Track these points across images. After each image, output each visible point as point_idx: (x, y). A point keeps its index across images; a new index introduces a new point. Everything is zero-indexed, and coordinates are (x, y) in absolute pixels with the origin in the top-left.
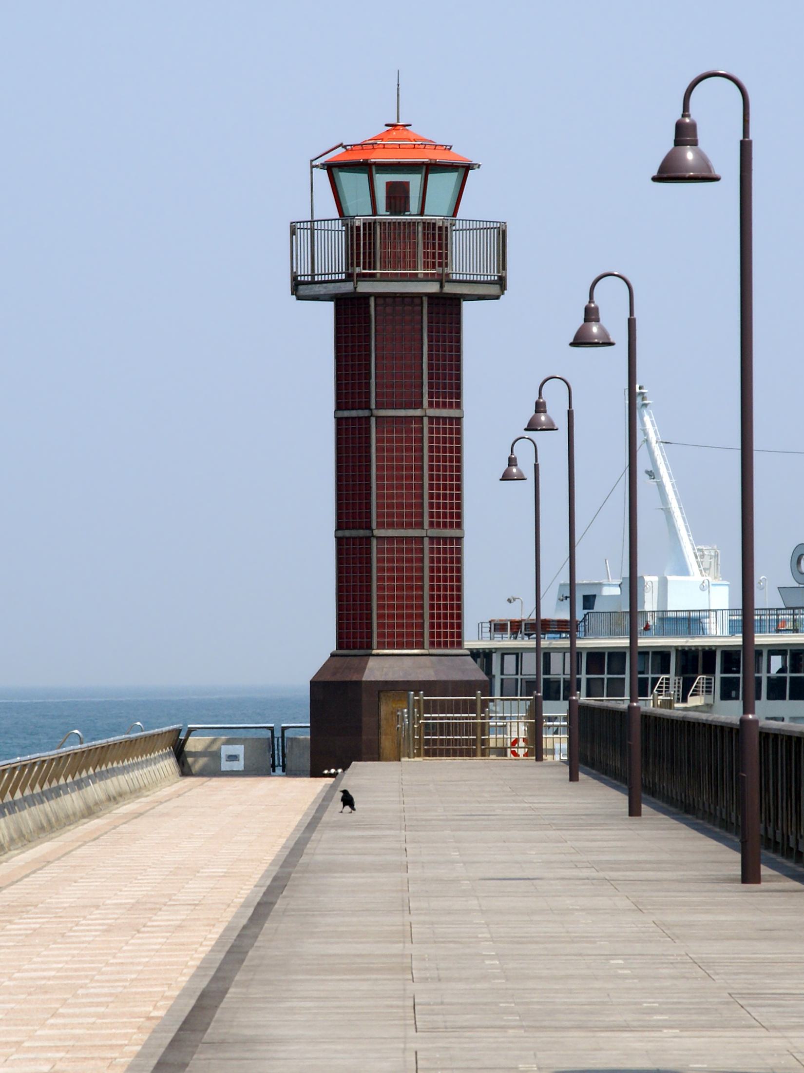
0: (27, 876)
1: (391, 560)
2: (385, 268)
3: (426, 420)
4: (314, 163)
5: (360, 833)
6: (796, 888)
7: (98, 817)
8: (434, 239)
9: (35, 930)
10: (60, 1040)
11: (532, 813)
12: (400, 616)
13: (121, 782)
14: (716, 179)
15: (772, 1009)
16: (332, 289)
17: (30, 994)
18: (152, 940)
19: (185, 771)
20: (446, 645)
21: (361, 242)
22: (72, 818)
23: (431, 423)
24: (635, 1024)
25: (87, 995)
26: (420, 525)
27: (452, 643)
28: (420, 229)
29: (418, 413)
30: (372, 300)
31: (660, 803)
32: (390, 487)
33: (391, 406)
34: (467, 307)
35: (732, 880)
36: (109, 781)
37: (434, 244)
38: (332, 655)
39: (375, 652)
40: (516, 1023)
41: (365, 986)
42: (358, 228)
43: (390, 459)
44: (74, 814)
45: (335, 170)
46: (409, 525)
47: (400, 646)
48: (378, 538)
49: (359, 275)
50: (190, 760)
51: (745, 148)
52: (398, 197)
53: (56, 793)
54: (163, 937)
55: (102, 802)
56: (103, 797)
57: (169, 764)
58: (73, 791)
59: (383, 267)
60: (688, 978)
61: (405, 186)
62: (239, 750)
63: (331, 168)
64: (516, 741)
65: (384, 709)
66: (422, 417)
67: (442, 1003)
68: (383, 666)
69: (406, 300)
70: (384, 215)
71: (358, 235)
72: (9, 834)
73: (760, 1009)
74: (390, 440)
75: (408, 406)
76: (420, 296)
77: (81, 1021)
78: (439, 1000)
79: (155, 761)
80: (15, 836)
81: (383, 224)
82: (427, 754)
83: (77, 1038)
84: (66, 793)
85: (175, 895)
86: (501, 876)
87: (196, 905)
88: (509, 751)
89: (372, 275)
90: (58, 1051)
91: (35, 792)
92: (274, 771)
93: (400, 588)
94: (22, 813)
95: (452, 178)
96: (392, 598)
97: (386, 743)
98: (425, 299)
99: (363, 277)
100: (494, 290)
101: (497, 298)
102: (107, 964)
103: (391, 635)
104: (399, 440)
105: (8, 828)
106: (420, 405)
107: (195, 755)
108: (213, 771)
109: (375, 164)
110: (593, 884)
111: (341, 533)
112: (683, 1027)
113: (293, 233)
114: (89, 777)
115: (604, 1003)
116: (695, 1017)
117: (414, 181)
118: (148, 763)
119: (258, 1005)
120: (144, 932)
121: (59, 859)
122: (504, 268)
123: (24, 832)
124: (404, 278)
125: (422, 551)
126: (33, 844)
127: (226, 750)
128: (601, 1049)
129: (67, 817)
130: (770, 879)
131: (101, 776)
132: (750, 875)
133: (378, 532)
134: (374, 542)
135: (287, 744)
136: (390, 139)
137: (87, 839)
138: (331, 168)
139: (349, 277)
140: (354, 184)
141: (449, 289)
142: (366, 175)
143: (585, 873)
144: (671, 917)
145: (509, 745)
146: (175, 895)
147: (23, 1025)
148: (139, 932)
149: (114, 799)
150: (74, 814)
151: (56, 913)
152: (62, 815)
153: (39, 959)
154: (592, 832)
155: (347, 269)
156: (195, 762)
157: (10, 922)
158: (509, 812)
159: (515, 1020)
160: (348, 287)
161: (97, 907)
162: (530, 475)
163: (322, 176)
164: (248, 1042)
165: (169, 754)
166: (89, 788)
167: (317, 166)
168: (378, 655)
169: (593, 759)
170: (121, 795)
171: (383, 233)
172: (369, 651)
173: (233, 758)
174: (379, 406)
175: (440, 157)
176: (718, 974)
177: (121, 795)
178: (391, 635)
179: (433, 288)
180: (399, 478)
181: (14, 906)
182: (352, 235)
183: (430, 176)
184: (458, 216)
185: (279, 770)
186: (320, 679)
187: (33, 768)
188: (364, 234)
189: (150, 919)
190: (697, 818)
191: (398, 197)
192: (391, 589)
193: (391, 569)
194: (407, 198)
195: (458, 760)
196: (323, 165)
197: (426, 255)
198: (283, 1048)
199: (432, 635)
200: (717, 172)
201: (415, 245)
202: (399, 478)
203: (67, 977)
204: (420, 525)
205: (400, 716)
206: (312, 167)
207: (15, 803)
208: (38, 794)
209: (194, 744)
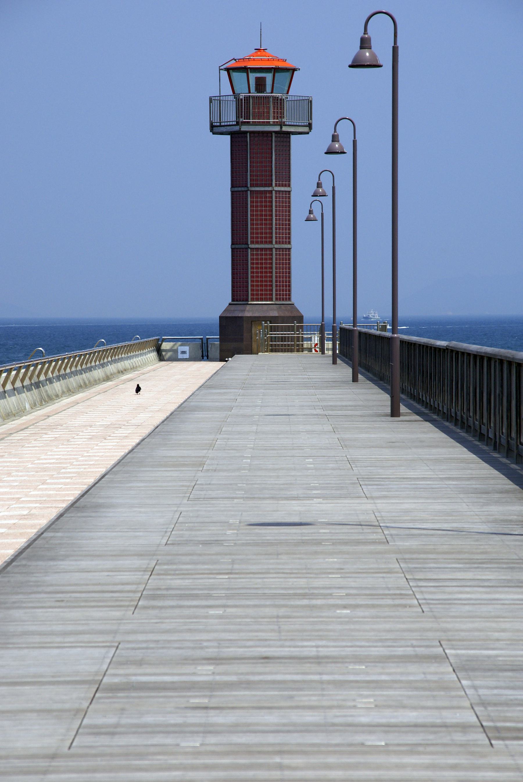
0: (64, 410)
1: (257, 259)
2: (254, 119)
3: (274, 192)
4: (221, 68)
5: (219, 391)
6: (416, 419)
7: (111, 381)
8: (278, 105)
9: (56, 438)
10: (40, 497)
11: (308, 380)
12: (261, 286)
13: (126, 364)
14: (380, 66)
15: (375, 487)
16: (229, 129)
17: (37, 472)
18: (108, 444)
19: (161, 358)
20: (283, 300)
21: (243, 106)
22: (98, 381)
23: (276, 194)
24: (302, 496)
25: (65, 473)
26: (271, 242)
27: (286, 299)
28: (271, 100)
29: (270, 189)
30: (248, 134)
31: (371, 375)
32: (257, 224)
33: (257, 185)
34: (293, 137)
35: (387, 415)
36: (119, 364)
37: (278, 107)
38: (230, 304)
39: (250, 303)
40: (241, 496)
41: (175, 474)
42: (242, 99)
43: (257, 211)
44: (99, 379)
45: (231, 71)
46: (266, 243)
47: (262, 300)
48: (251, 249)
49: (242, 122)
50: (164, 353)
51: (395, 50)
52: (260, 85)
53: (90, 369)
54: (115, 442)
55: (114, 374)
56: (115, 371)
57: (153, 355)
58: (99, 368)
59: (253, 118)
60: (340, 469)
61: (264, 79)
62: (186, 349)
63: (228, 70)
64: (317, 344)
65: (253, 330)
66: (272, 191)
67: (210, 484)
68: (254, 309)
69: (260, 134)
70: (254, 93)
71: (242, 103)
72: (62, 389)
73: (369, 487)
74: (257, 202)
75: (266, 185)
76: (271, 132)
77: (55, 486)
78: (209, 482)
79: (145, 354)
80: (65, 390)
81: (253, 97)
82: (272, 351)
83: (49, 496)
84: (95, 369)
85: (131, 420)
86: (276, 413)
87: (139, 425)
88: (313, 349)
89: (248, 122)
90: (36, 503)
91: (78, 369)
92: (203, 358)
93: (262, 272)
94: (70, 379)
95: (288, 75)
96: (257, 277)
97: (254, 346)
98: (274, 134)
99: (244, 123)
100: (306, 129)
101: (308, 133)
102: (82, 456)
103: (257, 295)
104: (261, 202)
105: (61, 386)
106: (271, 185)
107: (166, 351)
108: (174, 359)
109: (250, 68)
110: (318, 418)
111: (234, 246)
112: (324, 497)
113: (211, 101)
114: (108, 362)
115: (291, 484)
116: (333, 492)
117: (269, 77)
118: (141, 355)
119: (116, 485)
120: (108, 440)
121: (84, 401)
122: (311, 119)
123: (71, 388)
124: (263, 124)
125: (272, 255)
126: (74, 394)
127: (181, 349)
128: (278, 511)
129: (95, 381)
130: (405, 415)
131: (115, 361)
132: (395, 413)
133: (250, 246)
134: (249, 250)
135: (210, 346)
136: (257, 56)
137: (101, 392)
138: (228, 70)
139: (238, 123)
140: (239, 78)
141: (285, 129)
142: (246, 74)
143: (318, 411)
144: (347, 436)
145: (313, 346)
146: (131, 420)
147: (26, 489)
148: (105, 439)
149: (122, 372)
150: (99, 379)
151: (70, 429)
152: (92, 380)
153: (97, 447)
154: (331, 390)
155: (236, 119)
156: (166, 355)
157: (46, 434)
158: (297, 380)
159: (242, 494)
160: (236, 128)
161: (91, 426)
162: (319, 218)
163: (225, 74)
164: (97, 507)
165: (153, 351)
166: (108, 367)
167: (222, 69)
168: (251, 304)
169: (347, 353)
170: (125, 370)
171: (254, 103)
172: (247, 302)
173: (184, 352)
174: (252, 185)
175: (281, 65)
176: (356, 467)
177: (125, 370)
178: (257, 295)
179: (277, 128)
180: (261, 220)
181: (51, 426)
182: (239, 103)
183: (276, 74)
184: (290, 94)
185: (205, 358)
186: (224, 315)
187: (70, 359)
188: (245, 102)
189: (114, 433)
190: (385, 383)
191: (260, 85)
192: (257, 273)
193: (257, 264)
194: (265, 85)
195: (286, 354)
196: (225, 68)
197: (274, 112)
198: (113, 510)
199: (276, 295)
200: (380, 62)
201: (269, 108)
202: (261, 220)
203: (60, 463)
204: (271, 242)
205: (259, 332)
206: (220, 70)
207: (66, 374)
208: (80, 370)
209: (166, 346)
